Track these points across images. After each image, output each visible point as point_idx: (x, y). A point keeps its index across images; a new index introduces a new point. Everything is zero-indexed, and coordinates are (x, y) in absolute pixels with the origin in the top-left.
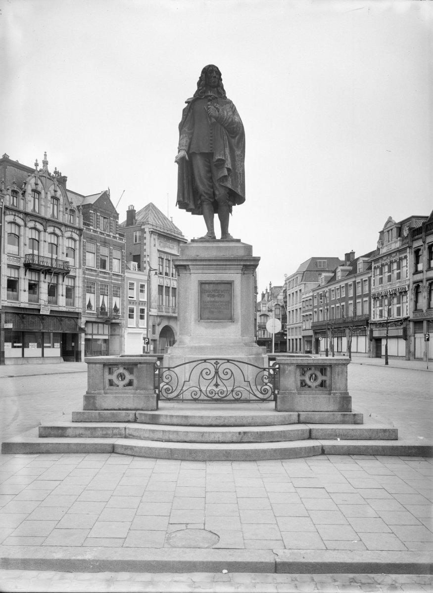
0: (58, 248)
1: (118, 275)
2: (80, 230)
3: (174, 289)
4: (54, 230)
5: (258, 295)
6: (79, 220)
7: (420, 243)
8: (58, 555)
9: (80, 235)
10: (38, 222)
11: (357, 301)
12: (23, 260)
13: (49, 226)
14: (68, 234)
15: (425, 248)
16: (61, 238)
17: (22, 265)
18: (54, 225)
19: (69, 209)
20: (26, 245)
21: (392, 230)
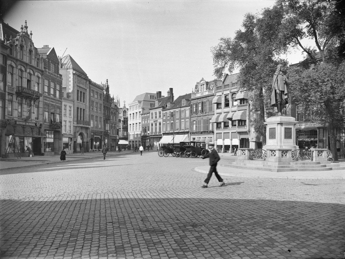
0: (13, 76)
1: (59, 101)
2: (42, 71)
3: (84, 110)
4: (21, 67)
5: (290, 177)
6: (42, 65)
7: (220, 94)
8: (330, 142)
9: (42, 75)
10: (13, 62)
11: (182, 121)
12: (15, 90)
13: (9, 60)
14: (19, 67)
15: (223, 96)
16: (33, 76)
17: (14, 93)
18: (12, 60)
19: (37, 58)
20: (17, 80)
21: (203, 85)
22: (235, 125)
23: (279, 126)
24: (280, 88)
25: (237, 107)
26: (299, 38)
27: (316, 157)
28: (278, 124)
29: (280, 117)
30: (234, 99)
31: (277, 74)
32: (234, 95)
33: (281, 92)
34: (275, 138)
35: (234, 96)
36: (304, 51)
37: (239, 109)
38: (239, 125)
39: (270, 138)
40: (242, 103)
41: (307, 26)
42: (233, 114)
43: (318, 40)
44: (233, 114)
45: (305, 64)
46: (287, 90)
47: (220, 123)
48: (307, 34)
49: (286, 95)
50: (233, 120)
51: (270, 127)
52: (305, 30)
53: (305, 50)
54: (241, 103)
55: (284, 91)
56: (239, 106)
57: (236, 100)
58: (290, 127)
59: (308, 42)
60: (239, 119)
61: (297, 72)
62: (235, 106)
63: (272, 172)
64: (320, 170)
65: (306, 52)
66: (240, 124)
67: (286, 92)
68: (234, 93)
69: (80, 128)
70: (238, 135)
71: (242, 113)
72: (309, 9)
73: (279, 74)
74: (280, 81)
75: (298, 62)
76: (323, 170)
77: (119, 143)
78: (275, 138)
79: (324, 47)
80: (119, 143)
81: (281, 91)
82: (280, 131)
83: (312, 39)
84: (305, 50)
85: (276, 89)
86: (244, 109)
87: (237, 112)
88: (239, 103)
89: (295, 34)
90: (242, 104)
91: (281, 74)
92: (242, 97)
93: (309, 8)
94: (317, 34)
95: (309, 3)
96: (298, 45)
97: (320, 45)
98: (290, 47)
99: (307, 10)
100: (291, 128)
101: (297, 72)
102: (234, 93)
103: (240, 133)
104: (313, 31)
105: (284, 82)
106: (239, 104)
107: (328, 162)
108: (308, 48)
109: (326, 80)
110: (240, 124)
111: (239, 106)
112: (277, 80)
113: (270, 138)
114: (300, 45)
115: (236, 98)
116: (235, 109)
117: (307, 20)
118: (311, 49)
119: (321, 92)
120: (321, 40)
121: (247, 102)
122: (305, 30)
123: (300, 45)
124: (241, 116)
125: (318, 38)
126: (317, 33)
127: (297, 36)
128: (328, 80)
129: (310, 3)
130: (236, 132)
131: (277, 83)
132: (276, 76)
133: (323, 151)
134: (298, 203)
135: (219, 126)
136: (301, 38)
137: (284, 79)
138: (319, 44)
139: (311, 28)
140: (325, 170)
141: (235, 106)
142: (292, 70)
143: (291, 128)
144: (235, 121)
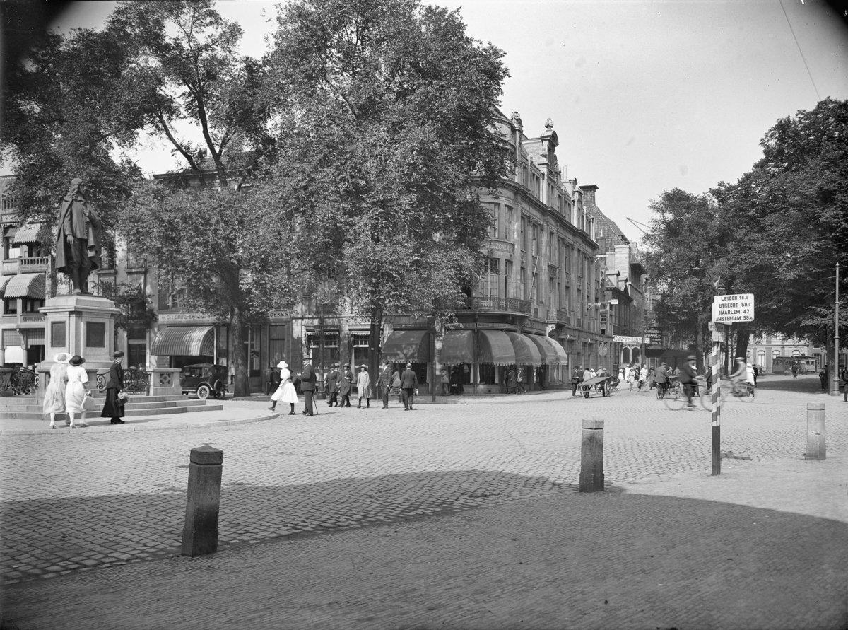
22: (14, 311)
23: (73, 317)
24: (78, 232)
25: (18, 262)
26: (165, 117)
28: (71, 313)
29: (76, 297)
30: (11, 241)
31: (70, 200)
32: (11, 230)
33: (81, 243)
34: (63, 344)
36: (176, 150)
38: (24, 309)
39: (53, 345)
40: (34, 254)
42: (7, 282)
43: (209, 130)
44: (7, 282)
45: (173, 181)
46: (95, 237)
48: (186, 114)
49: (92, 248)
51: (53, 320)
52: (181, 102)
53: (179, 148)
54: (30, 255)
55: (86, 241)
56: (23, 262)
57: (16, 245)
58: (101, 321)
59: (188, 131)
60: (24, 294)
62: (14, 261)
64: (157, 413)
65: (182, 152)
66: (29, 309)
67: (91, 242)
68: (12, 227)
70: (22, 339)
71: (33, 279)
72: (188, 57)
73: (76, 200)
74: (78, 216)
75: (165, 173)
76: (165, 413)
77: (111, 419)
78: (63, 344)
79: (222, 147)
80: (111, 419)
81: (81, 240)
82: (75, 330)
84: (179, 148)
85: (67, 232)
86: (39, 269)
87: (19, 276)
88: (27, 254)
89: (158, 109)
90: (35, 258)
91: (80, 201)
92: (33, 238)
93: (187, 55)
94: (207, 116)
95: (189, 42)
96: (164, 134)
97: (213, 141)
98: (142, 134)
99: (184, 58)
100: (103, 324)
101: (158, 195)
102: (12, 227)
103: (27, 332)
104: (197, 107)
105: (88, 220)
106: (26, 256)
107: (182, 397)
108: (185, 143)
109: (213, 221)
110: (29, 309)
111: (23, 262)
112: (71, 214)
113: (53, 345)
114: (169, 134)
115: (16, 240)
116: (14, 267)
118: (193, 147)
120: (216, 131)
121: (48, 253)
122: (181, 102)
123: (169, 134)
124: (31, 287)
125: (209, 125)
126: (208, 114)
127: (161, 113)
129: (192, 44)
130: (15, 329)
131: (71, 220)
132: (68, 204)
135: (11, 307)
136: (170, 119)
137: (87, 214)
138: (212, 139)
140: (169, 413)
142: (146, 188)
143: (103, 324)
144: (14, 299)
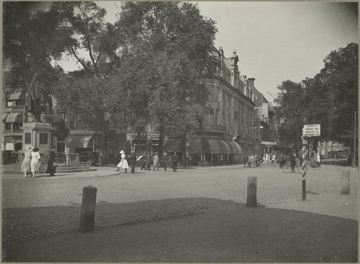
27: (68, 160)
28: (33, 129)
31: (34, 82)
35: (8, 96)
36: (78, 62)
37: (14, 111)
41: (81, 38)
42: (7, 116)
43: (92, 53)
44: (7, 116)
46: (44, 98)
47: (10, 123)
49: (42, 102)
50: (6, 122)
53: (79, 60)
54: (16, 105)
55: (40, 99)
57: (11, 101)
58: (46, 133)
59: (84, 54)
61: (70, 80)
63: (352, 168)
66: (16, 128)
67: (42, 100)
69: (211, 86)
72: (83, 23)
73: (36, 82)
83: (87, 51)
84: (79, 60)
85: (32, 96)
91: (38, 83)
93: (83, 22)
96: (73, 55)
97: (94, 58)
98: (64, 55)
100: (47, 134)
101: (70, 80)
104: (87, 43)
108: (82, 59)
109: (94, 91)
110: (16, 128)
113: (26, 143)
117: (82, 32)
119: (90, 101)
126: (92, 46)
128: (95, 92)
130: (10, 136)
133: (76, 155)
134: (131, 204)
135: (8, 127)
138: (93, 57)
139: (85, 41)
141: (10, 107)
143: (47, 134)
